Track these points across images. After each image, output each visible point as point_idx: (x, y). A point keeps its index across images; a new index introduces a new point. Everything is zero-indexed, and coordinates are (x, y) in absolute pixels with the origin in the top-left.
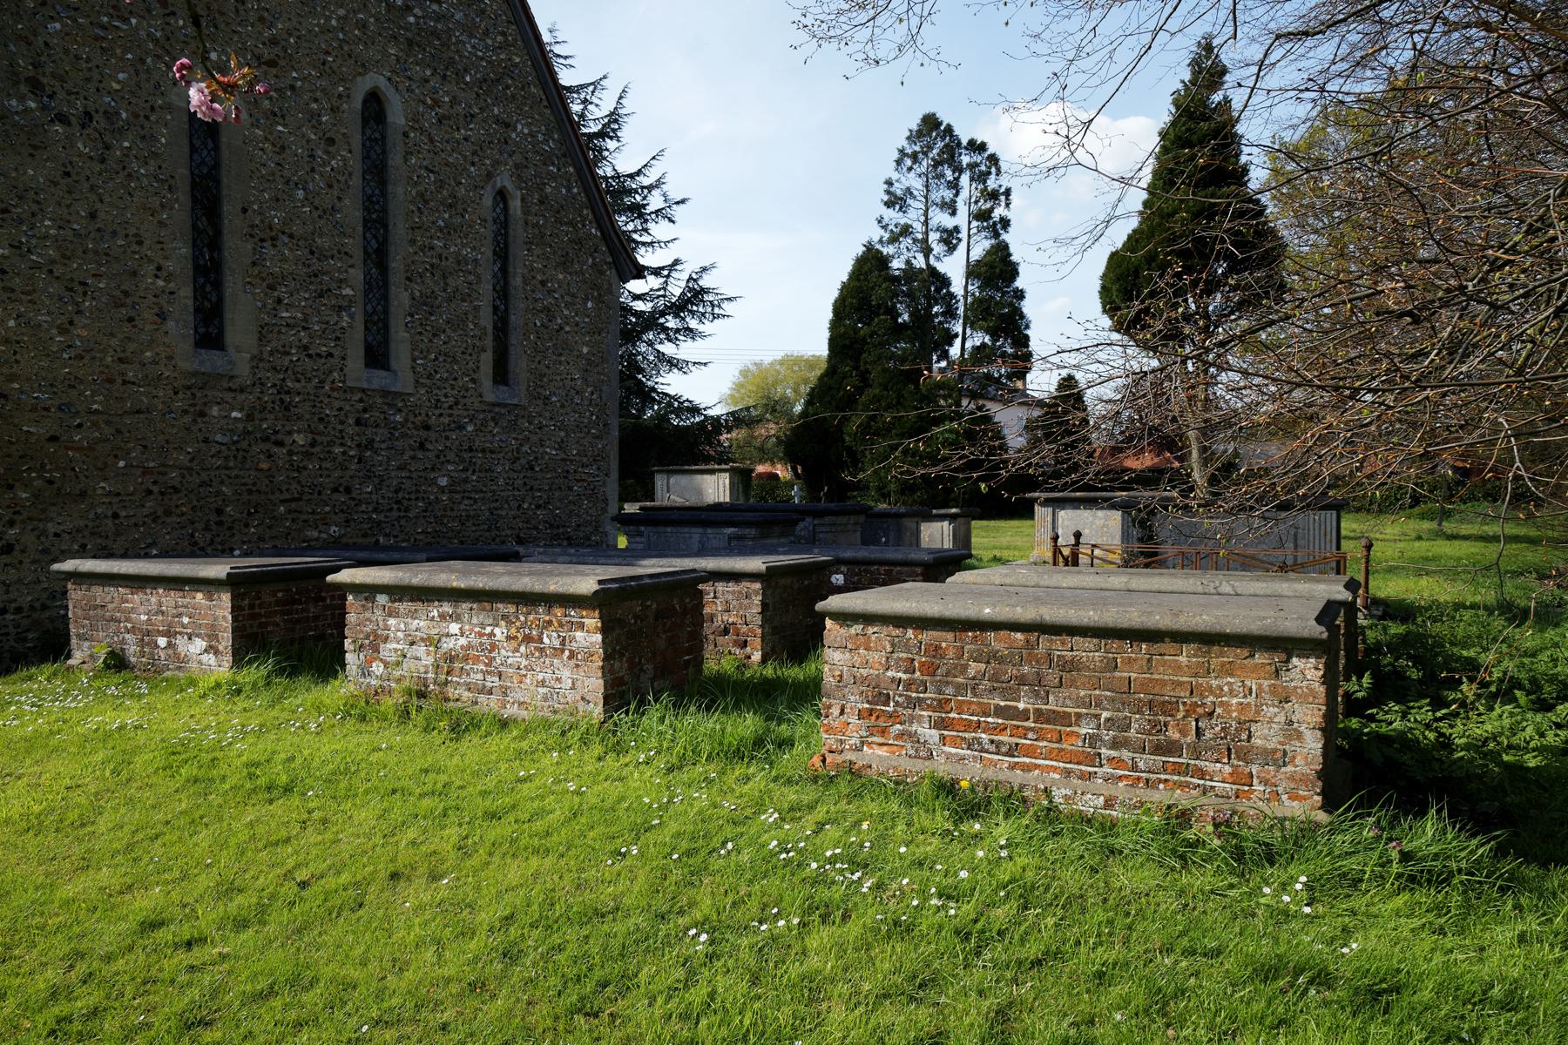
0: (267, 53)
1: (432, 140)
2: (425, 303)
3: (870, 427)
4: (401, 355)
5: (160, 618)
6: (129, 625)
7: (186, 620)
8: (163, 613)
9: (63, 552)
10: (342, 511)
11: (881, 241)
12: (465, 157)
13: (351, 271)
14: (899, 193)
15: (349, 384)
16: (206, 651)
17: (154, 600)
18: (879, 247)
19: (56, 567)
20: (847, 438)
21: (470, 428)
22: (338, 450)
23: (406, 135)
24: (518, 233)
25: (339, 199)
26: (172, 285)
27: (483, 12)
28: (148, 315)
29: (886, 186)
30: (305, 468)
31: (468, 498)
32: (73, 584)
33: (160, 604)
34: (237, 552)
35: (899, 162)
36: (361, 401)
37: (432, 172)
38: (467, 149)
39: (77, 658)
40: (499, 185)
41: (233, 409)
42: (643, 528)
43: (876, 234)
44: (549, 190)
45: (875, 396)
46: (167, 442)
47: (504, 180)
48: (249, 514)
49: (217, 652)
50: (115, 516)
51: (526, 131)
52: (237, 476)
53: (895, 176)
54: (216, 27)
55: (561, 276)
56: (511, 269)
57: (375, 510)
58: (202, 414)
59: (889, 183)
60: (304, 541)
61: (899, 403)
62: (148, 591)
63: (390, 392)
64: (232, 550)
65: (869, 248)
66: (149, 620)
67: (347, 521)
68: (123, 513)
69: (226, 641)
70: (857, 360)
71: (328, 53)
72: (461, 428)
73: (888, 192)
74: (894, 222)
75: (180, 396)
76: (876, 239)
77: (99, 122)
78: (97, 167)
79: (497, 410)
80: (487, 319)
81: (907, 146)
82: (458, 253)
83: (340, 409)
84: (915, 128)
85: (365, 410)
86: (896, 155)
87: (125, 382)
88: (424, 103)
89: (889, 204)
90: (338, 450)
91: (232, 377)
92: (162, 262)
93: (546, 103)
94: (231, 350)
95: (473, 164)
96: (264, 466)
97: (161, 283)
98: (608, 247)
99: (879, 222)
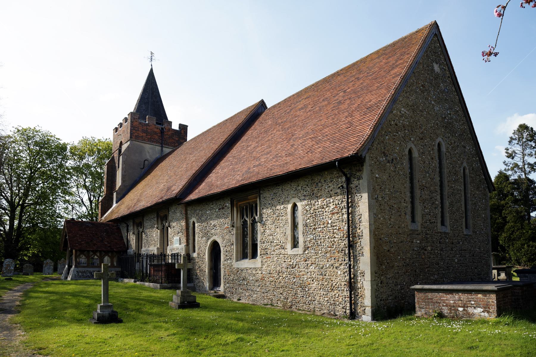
0: (421, 136)
1: (451, 155)
2: (451, 204)
3: (511, 237)
4: (448, 222)
5: (460, 302)
6: (444, 304)
7: (473, 303)
8: (461, 301)
9: (472, 280)
10: (437, 271)
11: (505, 170)
12: (457, 158)
13: (437, 196)
14: (510, 152)
15: (439, 231)
16: (483, 312)
17: (457, 297)
18: (504, 172)
19: (413, 287)
20: (501, 242)
21: (461, 243)
22: (436, 251)
23: (446, 154)
24: (468, 180)
25: (434, 175)
26: (407, 205)
27: (459, 115)
28: (403, 214)
29: (506, 151)
30: (430, 257)
31: (461, 266)
32: (417, 292)
33: (460, 298)
34: (419, 283)
35: (510, 142)
36: (440, 236)
37: (451, 164)
38: (457, 155)
39: (419, 314)
40: (464, 166)
41: (418, 240)
42: (527, 275)
43: (503, 167)
44: (474, 165)
45: (512, 226)
46: (406, 250)
47: (465, 164)
48: (421, 272)
49: (488, 312)
50: (398, 273)
51: (468, 148)
52: (419, 260)
53: (509, 147)
54: (413, 131)
55: (477, 192)
56: (467, 192)
57: (444, 270)
58: (412, 242)
59: (507, 149)
60: (430, 280)
61: (522, 228)
62: (454, 294)
63: (446, 233)
64: (418, 283)
65: (501, 173)
66: (454, 303)
67: (438, 274)
68: (399, 272)
69: (494, 308)
70: (501, 213)
71: (431, 134)
72: (459, 243)
73: (507, 153)
74: (509, 163)
75: (409, 237)
76: (503, 169)
77: (395, 161)
78: (394, 173)
79: (466, 237)
80: (463, 209)
81: (513, 136)
82: (457, 188)
83: (436, 239)
84: (516, 129)
85: (441, 239)
86: (509, 139)
87: (399, 234)
88: (449, 144)
89: (508, 157)
90: (436, 251)
91: (418, 230)
92: (405, 198)
93: (472, 139)
94: (417, 222)
95: (459, 160)
96: (423, 257)
97: (405, 204)
98: (487, 182)
99: (504, 163)
